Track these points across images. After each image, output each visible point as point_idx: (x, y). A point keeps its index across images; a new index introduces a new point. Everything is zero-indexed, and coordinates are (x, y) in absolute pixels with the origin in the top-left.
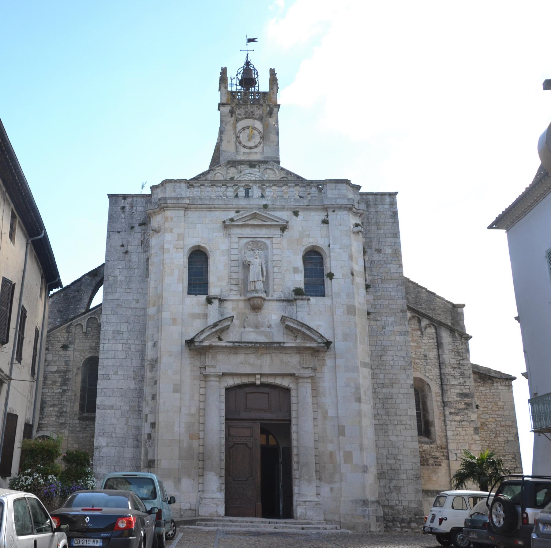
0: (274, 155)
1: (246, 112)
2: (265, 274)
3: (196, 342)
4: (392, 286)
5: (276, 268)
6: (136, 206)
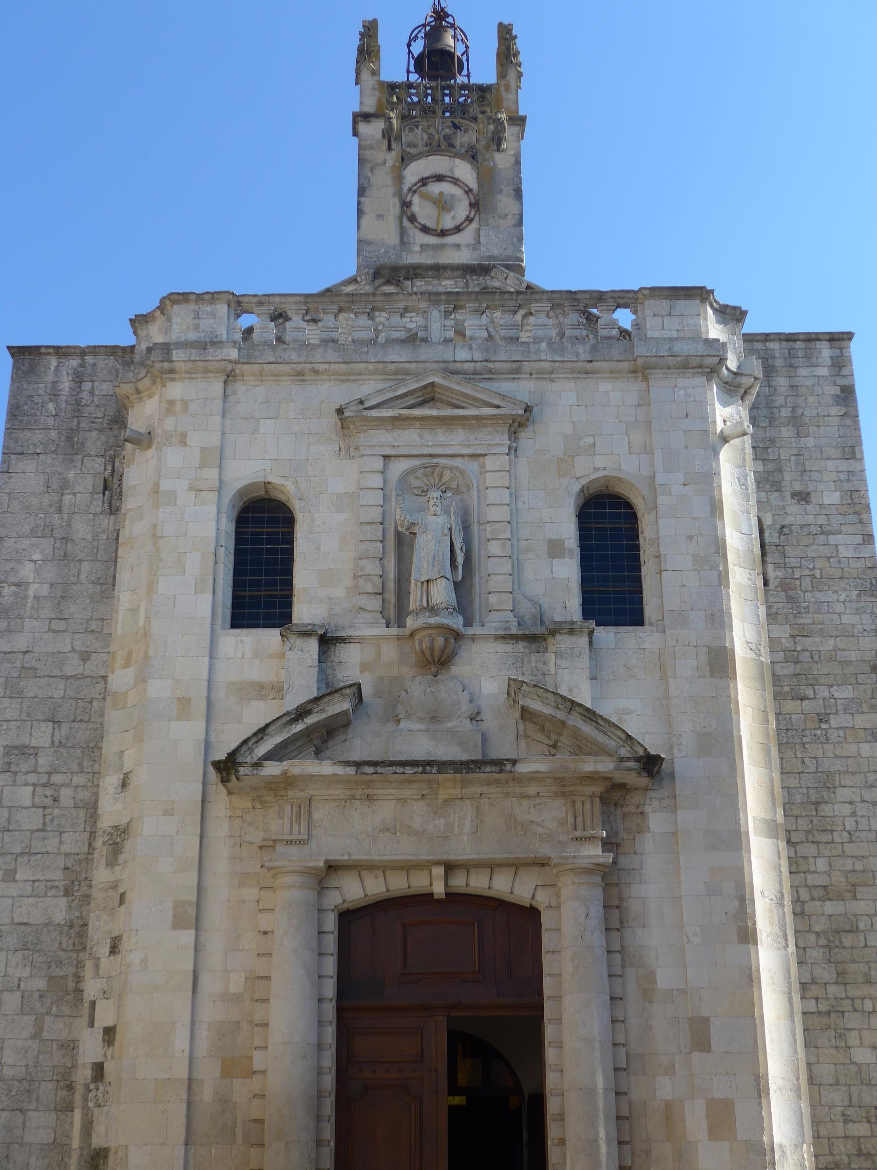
0: (510, 252)
1: (430, 136)
2: (460, 559)
3: (240, 764)
4: (842, 598)
5: (493, 542)
6: (93, 381)
